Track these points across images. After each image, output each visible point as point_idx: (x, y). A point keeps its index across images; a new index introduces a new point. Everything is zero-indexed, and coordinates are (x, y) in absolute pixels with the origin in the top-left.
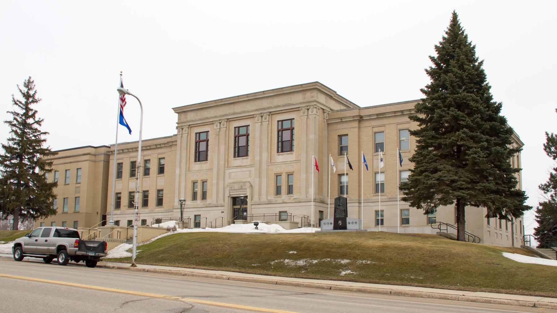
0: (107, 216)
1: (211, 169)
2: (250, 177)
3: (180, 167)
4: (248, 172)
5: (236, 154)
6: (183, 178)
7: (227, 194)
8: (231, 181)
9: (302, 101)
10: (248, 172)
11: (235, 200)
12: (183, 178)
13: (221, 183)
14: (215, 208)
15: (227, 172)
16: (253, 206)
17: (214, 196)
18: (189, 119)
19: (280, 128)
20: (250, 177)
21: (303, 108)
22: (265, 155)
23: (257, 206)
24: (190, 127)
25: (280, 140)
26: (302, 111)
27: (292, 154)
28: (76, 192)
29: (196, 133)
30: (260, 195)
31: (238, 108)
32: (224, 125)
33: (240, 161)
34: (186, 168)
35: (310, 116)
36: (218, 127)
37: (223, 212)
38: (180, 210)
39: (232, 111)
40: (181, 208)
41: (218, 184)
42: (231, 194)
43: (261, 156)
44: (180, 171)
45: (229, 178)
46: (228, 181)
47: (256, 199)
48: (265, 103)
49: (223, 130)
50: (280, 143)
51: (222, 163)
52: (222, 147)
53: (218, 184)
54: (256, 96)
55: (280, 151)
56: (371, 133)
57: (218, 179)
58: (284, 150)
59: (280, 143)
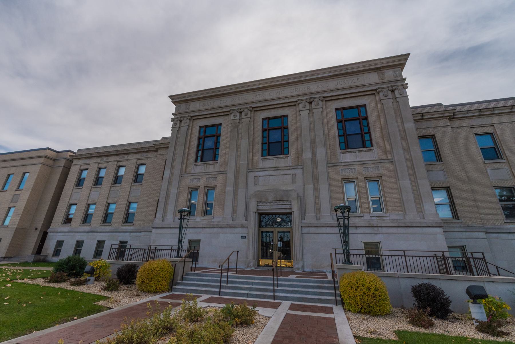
0: (49, 234)
1: (224, 172)
2: (294, 182)
3: (172, 168)
4: (290, 177)
5: (199, 158)
6: (175, 182)
7: (253, 207)
8: (259, 188)
9: (378, 81)
10: (290, 177)
11: (264, 218)
12: (175, 182)
13: (241, 192)
14: (228, 230)
15: (251, 175)
16: (305, 230)
17: (228, 211)
18: (191, 109)
19: (202, 134)
20: (294, 182)
21: (185, 118)
22: (321, 152)
23: (312, 230)
24: (193, 118)
25: (200, 148)
26: (233, 115)
27: (286, 157)
28: (12, 201)
29: (201, 127)
30: (318, 210)
31: (268, 95)
32: (246, 115)
33: (271, 162)
34: (181, 170)
35: (182, 128)
36: (238, 117)
37: (243, 237)
38: (177, 231)
39: (259, 98)
40: (181, 227)
41: (235, 193)
42: (260, 207)
43: (313, 154)
44: (172, 173)
45: (256, 184)
46: (253, 189)
47: (310, 218)
48: (314, 87)
49: (245, 121)
50: (200, 152)
51: (243, 162)
52: (244, 143)
53: (235, 193)
54: (301, 77)
55: (199, 160)
56: (115, 166)
57: (236, 185)
58: (204, 160)
59: (200, 152)
